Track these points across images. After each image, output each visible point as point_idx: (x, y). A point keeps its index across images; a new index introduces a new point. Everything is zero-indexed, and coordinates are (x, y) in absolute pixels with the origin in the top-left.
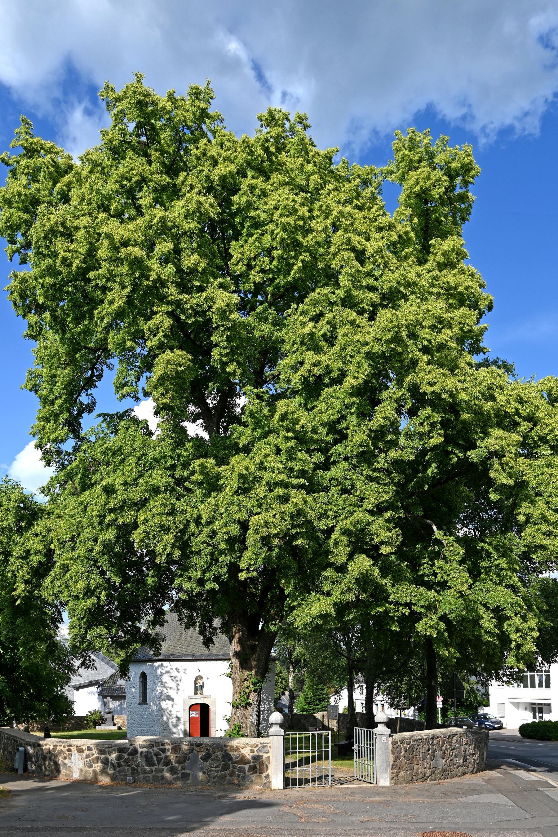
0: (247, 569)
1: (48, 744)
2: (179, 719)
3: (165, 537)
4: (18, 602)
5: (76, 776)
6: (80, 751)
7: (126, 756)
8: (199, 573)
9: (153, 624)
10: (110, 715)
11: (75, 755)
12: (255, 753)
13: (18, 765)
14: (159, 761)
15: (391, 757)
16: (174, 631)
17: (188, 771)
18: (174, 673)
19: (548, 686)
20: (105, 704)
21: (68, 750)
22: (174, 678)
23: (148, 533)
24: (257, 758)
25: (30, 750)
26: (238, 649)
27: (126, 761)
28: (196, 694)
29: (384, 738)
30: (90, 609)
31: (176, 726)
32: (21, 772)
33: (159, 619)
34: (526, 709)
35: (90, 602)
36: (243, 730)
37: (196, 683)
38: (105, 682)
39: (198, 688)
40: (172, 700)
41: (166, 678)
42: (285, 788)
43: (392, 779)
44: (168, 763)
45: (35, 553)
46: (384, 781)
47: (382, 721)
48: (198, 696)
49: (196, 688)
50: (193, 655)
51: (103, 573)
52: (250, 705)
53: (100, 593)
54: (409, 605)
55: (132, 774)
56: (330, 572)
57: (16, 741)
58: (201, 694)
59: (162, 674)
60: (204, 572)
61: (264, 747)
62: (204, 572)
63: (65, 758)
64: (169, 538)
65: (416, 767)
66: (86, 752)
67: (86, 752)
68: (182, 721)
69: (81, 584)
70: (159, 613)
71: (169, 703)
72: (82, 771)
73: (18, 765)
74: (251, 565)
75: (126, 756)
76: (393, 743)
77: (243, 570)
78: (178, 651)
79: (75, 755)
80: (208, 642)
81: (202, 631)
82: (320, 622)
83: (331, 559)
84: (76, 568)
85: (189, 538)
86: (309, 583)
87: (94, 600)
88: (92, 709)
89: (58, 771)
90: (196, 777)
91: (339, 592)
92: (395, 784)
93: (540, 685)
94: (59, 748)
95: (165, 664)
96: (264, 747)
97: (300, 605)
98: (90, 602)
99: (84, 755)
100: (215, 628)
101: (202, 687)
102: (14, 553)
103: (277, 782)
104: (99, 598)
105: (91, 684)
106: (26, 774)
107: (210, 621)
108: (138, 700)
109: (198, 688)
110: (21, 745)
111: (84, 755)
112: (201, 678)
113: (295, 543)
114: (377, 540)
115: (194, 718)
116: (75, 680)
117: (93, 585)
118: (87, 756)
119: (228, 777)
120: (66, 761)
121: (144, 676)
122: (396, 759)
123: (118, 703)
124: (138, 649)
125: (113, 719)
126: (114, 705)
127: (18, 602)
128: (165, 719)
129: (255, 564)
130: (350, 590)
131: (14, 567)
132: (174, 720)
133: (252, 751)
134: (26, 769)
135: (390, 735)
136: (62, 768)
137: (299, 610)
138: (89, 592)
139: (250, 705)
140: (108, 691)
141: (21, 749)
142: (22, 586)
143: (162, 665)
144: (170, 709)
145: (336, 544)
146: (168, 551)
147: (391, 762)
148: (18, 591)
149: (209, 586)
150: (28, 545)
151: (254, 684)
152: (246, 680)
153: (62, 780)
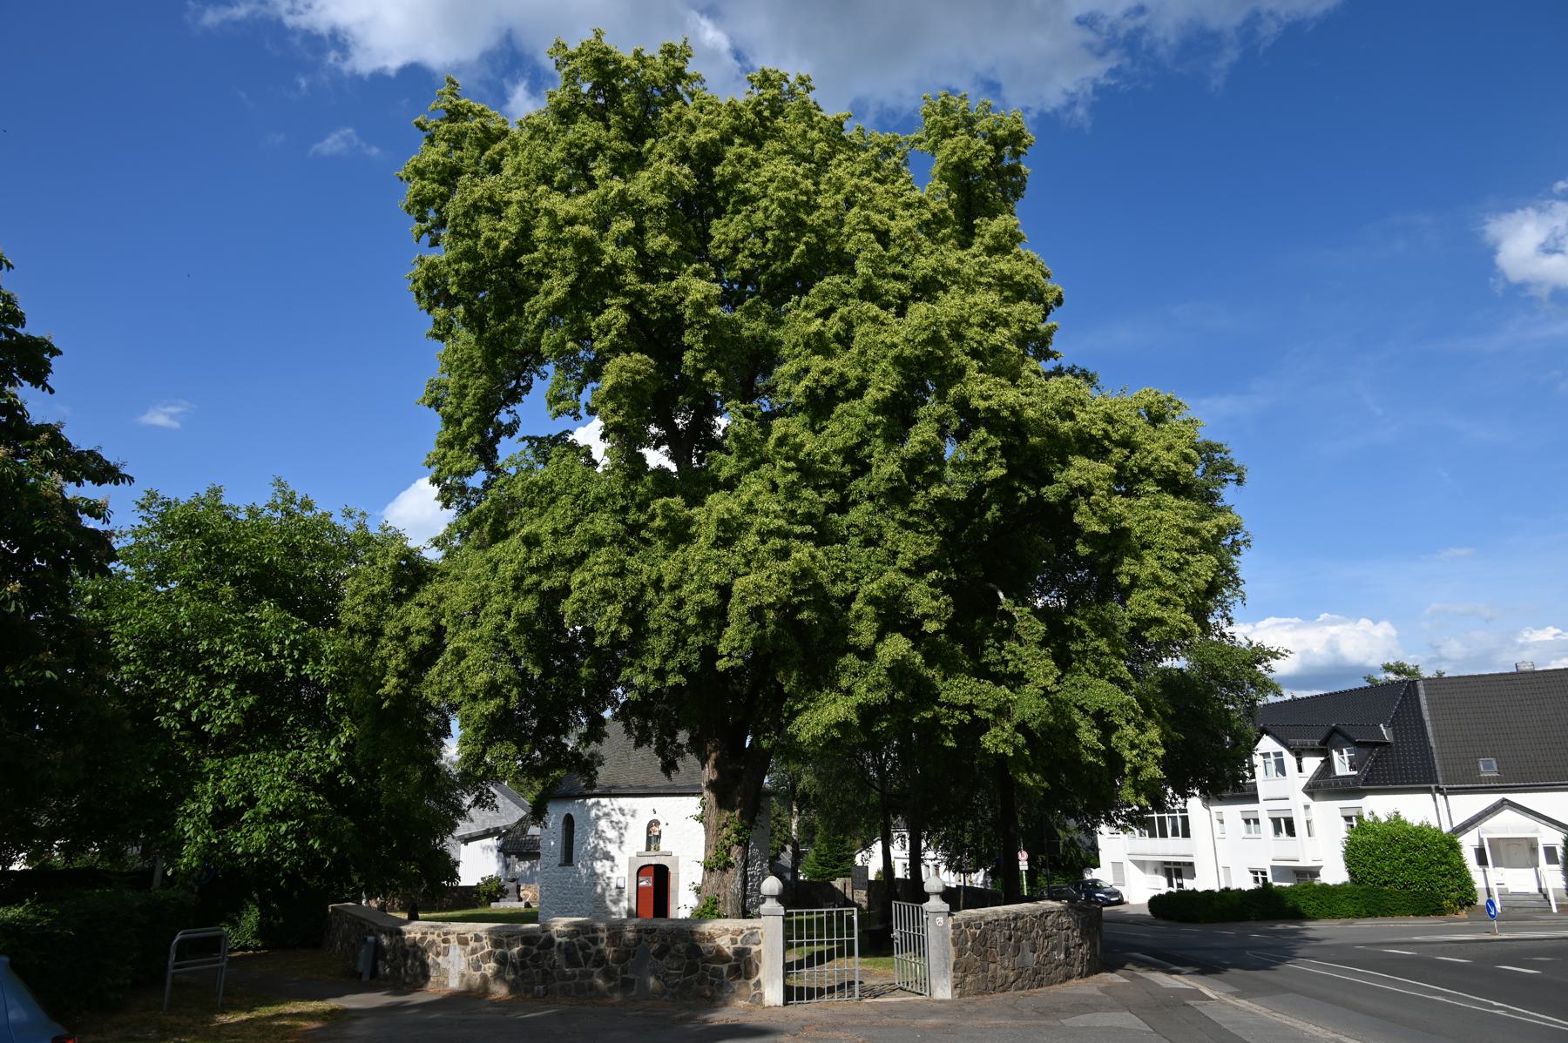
0: (729, 655)
1: (414, 930)
2: (620, 889)
3: (610, 608)
4: (385, 705)
5: (454, 984)
6: (463, 942)
7: (535, 951)
8: (657, 661)
9: (586, 738)
10: (513, 885)
11: (455, 950)
12: (739, 945)
13: (362, 966)
14: (587, 957)
15: (952, 951)
16: (618, 750)
17: (631, 976)
18: (616, 817)
19: (1186, 834)
20: (507, 866)
21: (445, 941)
22: (615, 825)
23: (585, 602)
24: (742, 953)
25: (385, 941)
26: (714, 777)
27: (535, 959)
28: (648, 849)
29: (940, 919)
30: (492, 714)
31: (616, 902)
32: (365, 978)
33: (596, 731)
34: (1156, 872)
35: (493, 705)
36: (721, 906)
37: (649, 832)
38: (509, 831)
39: (653, 840)
40: (612, 859)
41: (603, 824)
42: (785, 1004)
43: (955, 987)
44: (600, 960)
45: (418, 632)
46: (943, 990)
47: (936, 889)
48: (652, 852)
49: (649, 839)
50: (645, 787)
51: (516, 661)
52: (731, 865)
53: (510, 691)
54: (969, 708)
55: (543, 982)
56: (849, 659)
57: (363, 926)
58: (657, 849)
59: (598, 818)
60: (665, 659)
61: (752, 934)
62: (665, 659)
63: (438, 954)
64: (615, 610)
65: (992, 966)
66: (472, 944)
67: (472, 944)
68: (626, 895)
69: (483, 677)
70: (597, 724)
71: (608, 864)
72: (463, 975)
73: (362, 966)
74: (734, 649)
75: (535, 951)
76: (954, 927)
77: (722, 657)
78: (623, 780)
79: (455, 950)
80: (669, 767)
81: (660, 751)
82: (836, 733)
83: (852, 639)
84: (476, 653)
85: (645, 609)
86: (821, 677)
87: (499, 701)
88: (486, 874)
89: (426, 977)
90: (645, 984)
91: (864, 689)
92: (961, 995)
93: (1175, 833)
94: (429, 937)
95: (604, 801)
96: (752, 934)
97: (806, 708)
98: (493, 705)
99: (469, 948)
100: (680, 746)
101: (659, 837)
102: (387, 631)
103: (773, 994)
104: (507, 698)
105: (487, 834)
106: (373, 982)
107: (673, 735)
108: (558, 859)
109: (653, 840)
110: (371, 933)
111: (469, 948)
112: (657, 823)
113: (800, 617)
114: (917, 611)
115: (644, 888)
116: (464, 828)
117: (500, 678)
118: (474, 951)
119: (695, 986)
120: (440, 959)
121: (569, 821)
122: (960, 953)
123: (528, 864)
124: (563, 780)
125: (518, 891)
126: (521, 867)
127: (385, 705)
128: (599, 890)
129: (741, 647)
130: (879, 686)
131: (384, 653)
132: (614, 892)
133: (734, 941)
134: (374, 973)
135: (950, 914)
136: (433, 973)
137: (806, 716)
138: (493, 689)
139: (731, 865)
140: (514, 846)
141: (371, 939)
142: (394, 680)
143: (598, 803)
144: (609, 874)
145: (859, 617)
146: (613, 628)
147: (953, 960)
148: (387, 688)
149: (672, 680)
150: (409, 620)
151: (738, 832)
152: (725, 826)
153: (432, 991)
